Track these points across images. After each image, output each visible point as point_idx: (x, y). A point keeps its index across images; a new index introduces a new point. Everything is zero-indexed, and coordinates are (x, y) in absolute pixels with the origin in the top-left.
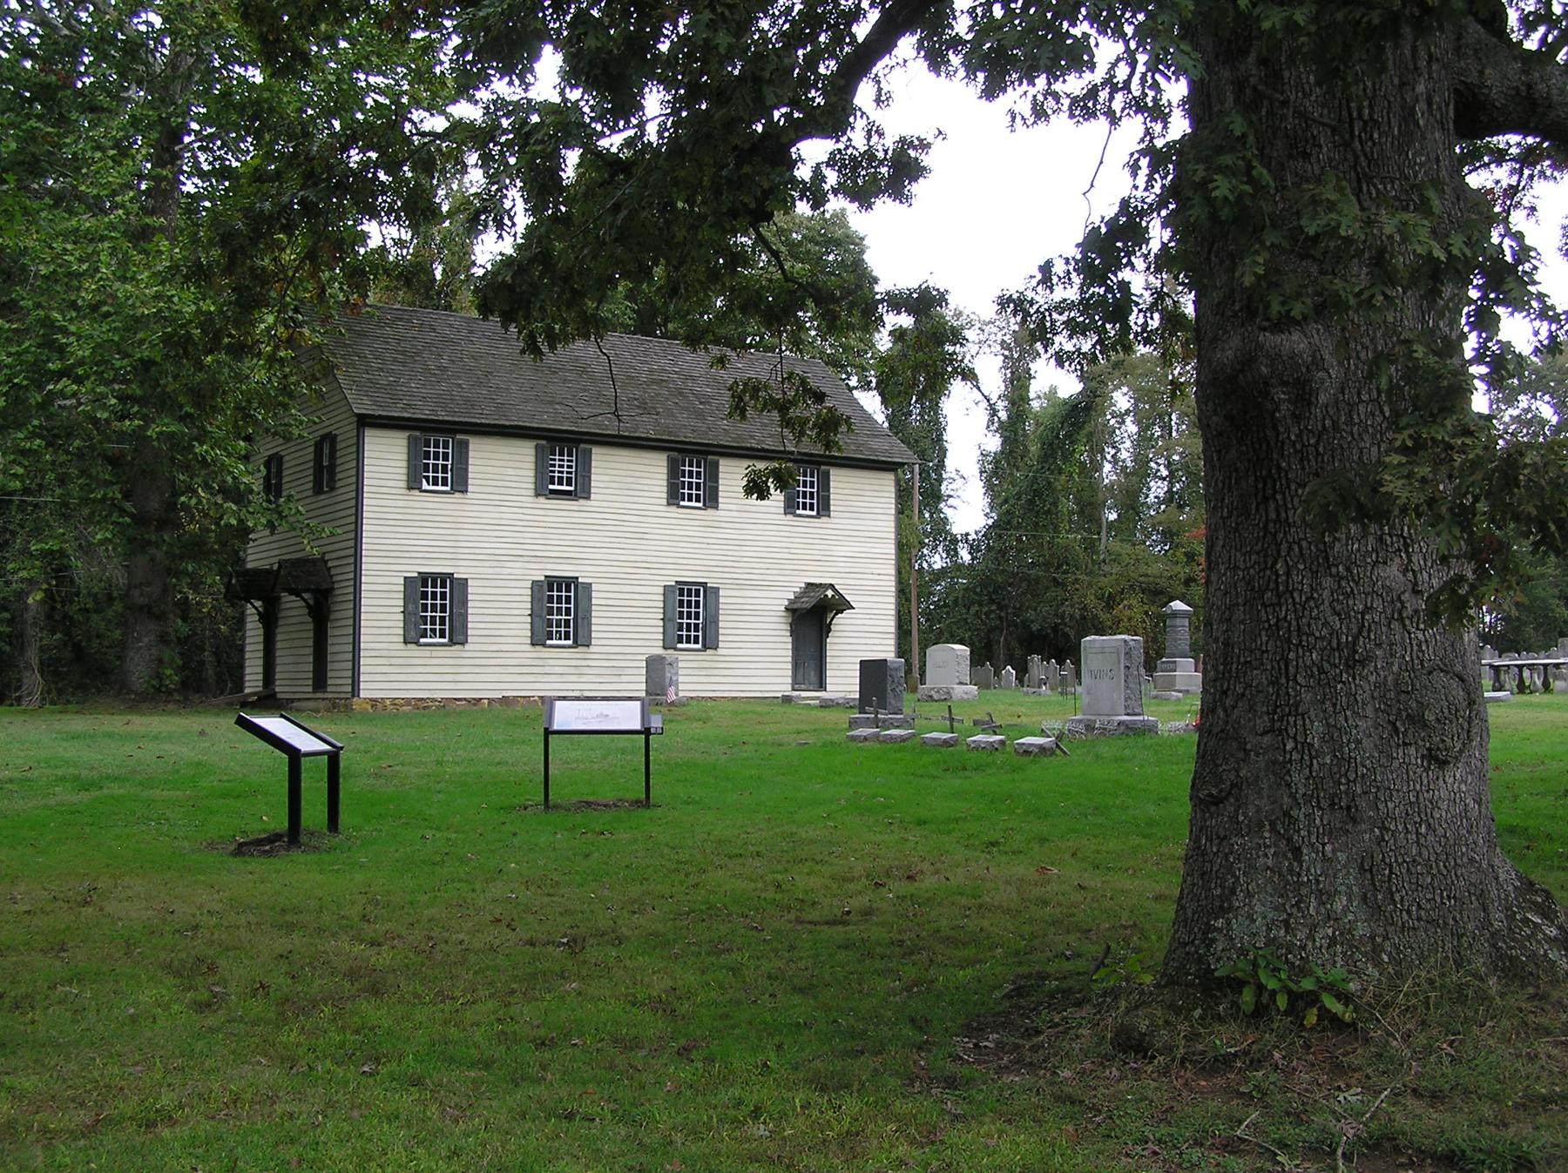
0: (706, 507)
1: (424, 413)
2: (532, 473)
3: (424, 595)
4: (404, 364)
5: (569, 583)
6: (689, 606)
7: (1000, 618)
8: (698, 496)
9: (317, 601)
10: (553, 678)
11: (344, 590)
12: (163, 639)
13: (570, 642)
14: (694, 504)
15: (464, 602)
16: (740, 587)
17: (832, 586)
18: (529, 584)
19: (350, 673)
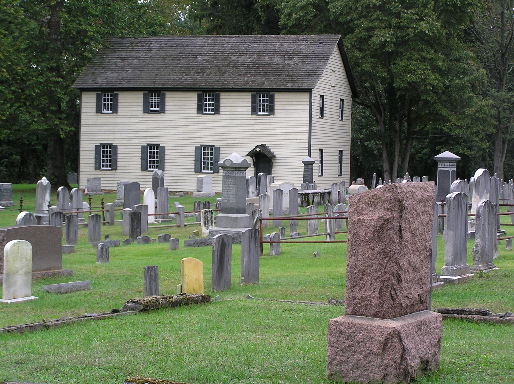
14: (265, 113)
15: (116, 154)
17: (257, 147)
18: (141, 147)
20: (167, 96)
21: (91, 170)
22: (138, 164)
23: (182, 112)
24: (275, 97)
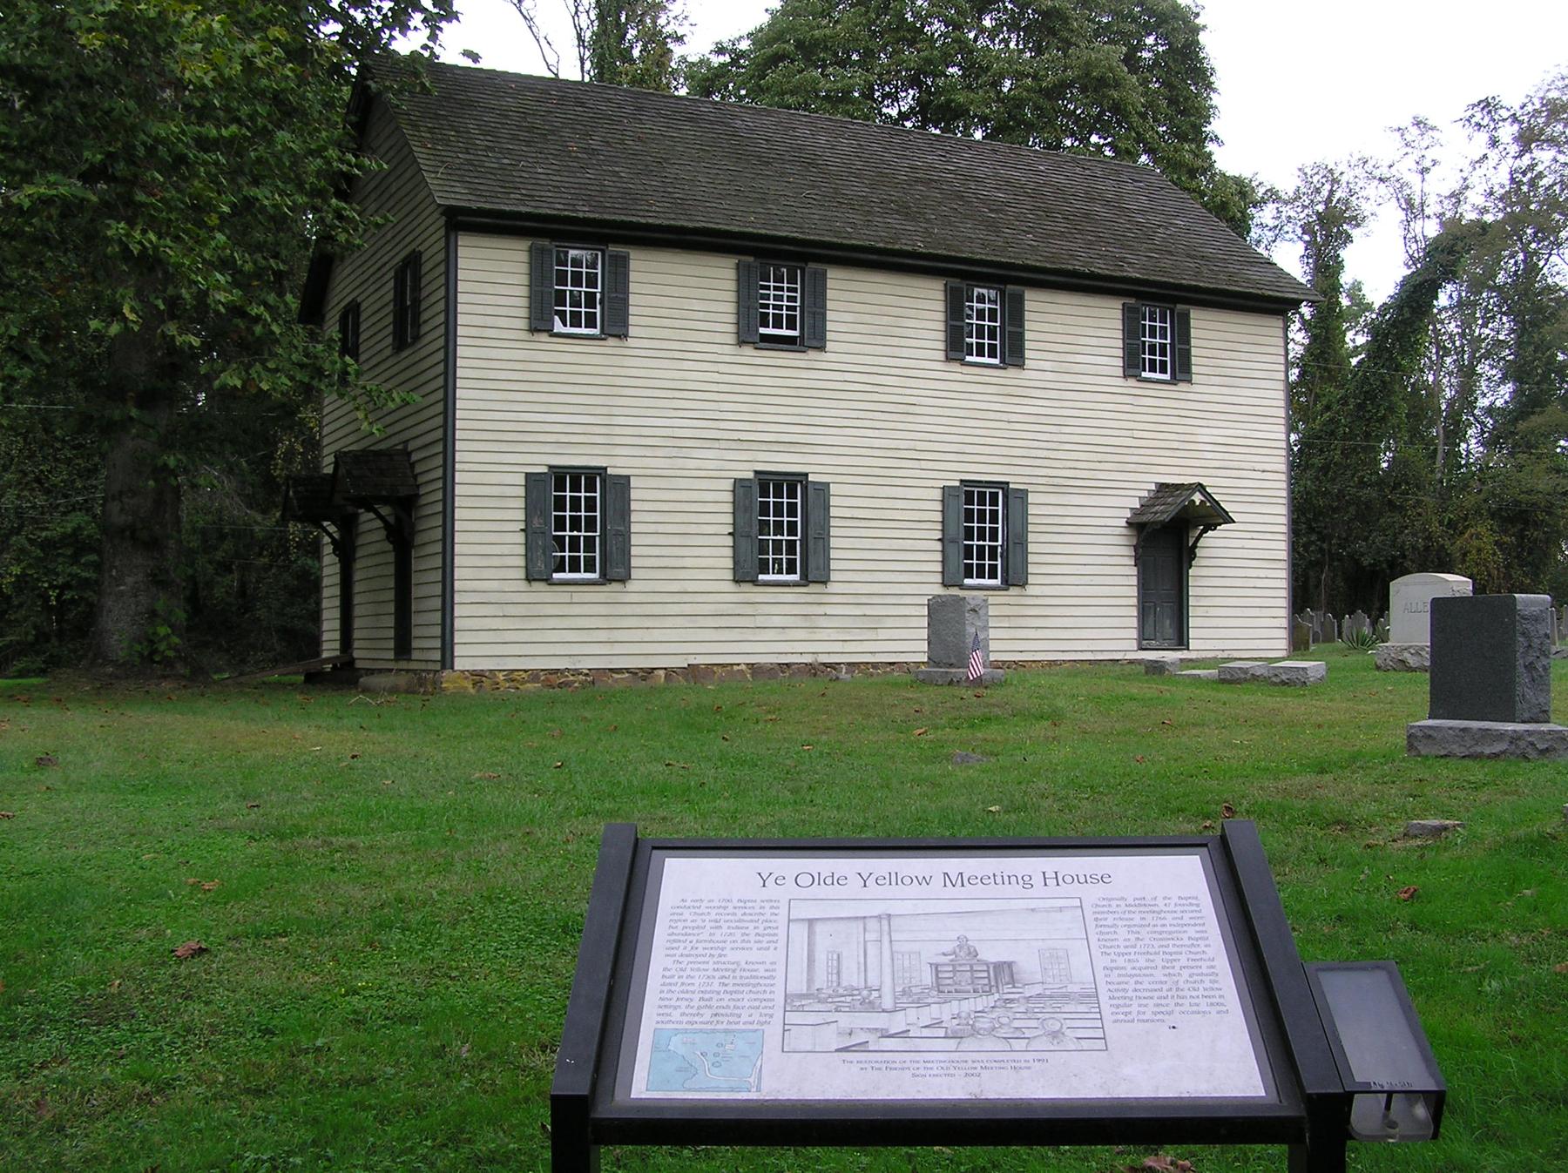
0: (1004, 365)
1: (554, 206)
2: (732, 308)
3: (560, 504)
4: (528, 143)
5: (792, 482)
6: (982, 519)
7: (1321, 550)
8: (992, 349)
9: (398, 519)
10: (770, 635)
11: (431, 496)
12: (158, 580)
13: (795, 577)
15: (625, 513)
16: (1058, 487)
17: (1201, 488)
18: (729, 485)
19: (437, 631)
20: (633, 264)
21: (507, 586)
22: (721, 557)
23: (888, 351)
24: (1028, 305)
